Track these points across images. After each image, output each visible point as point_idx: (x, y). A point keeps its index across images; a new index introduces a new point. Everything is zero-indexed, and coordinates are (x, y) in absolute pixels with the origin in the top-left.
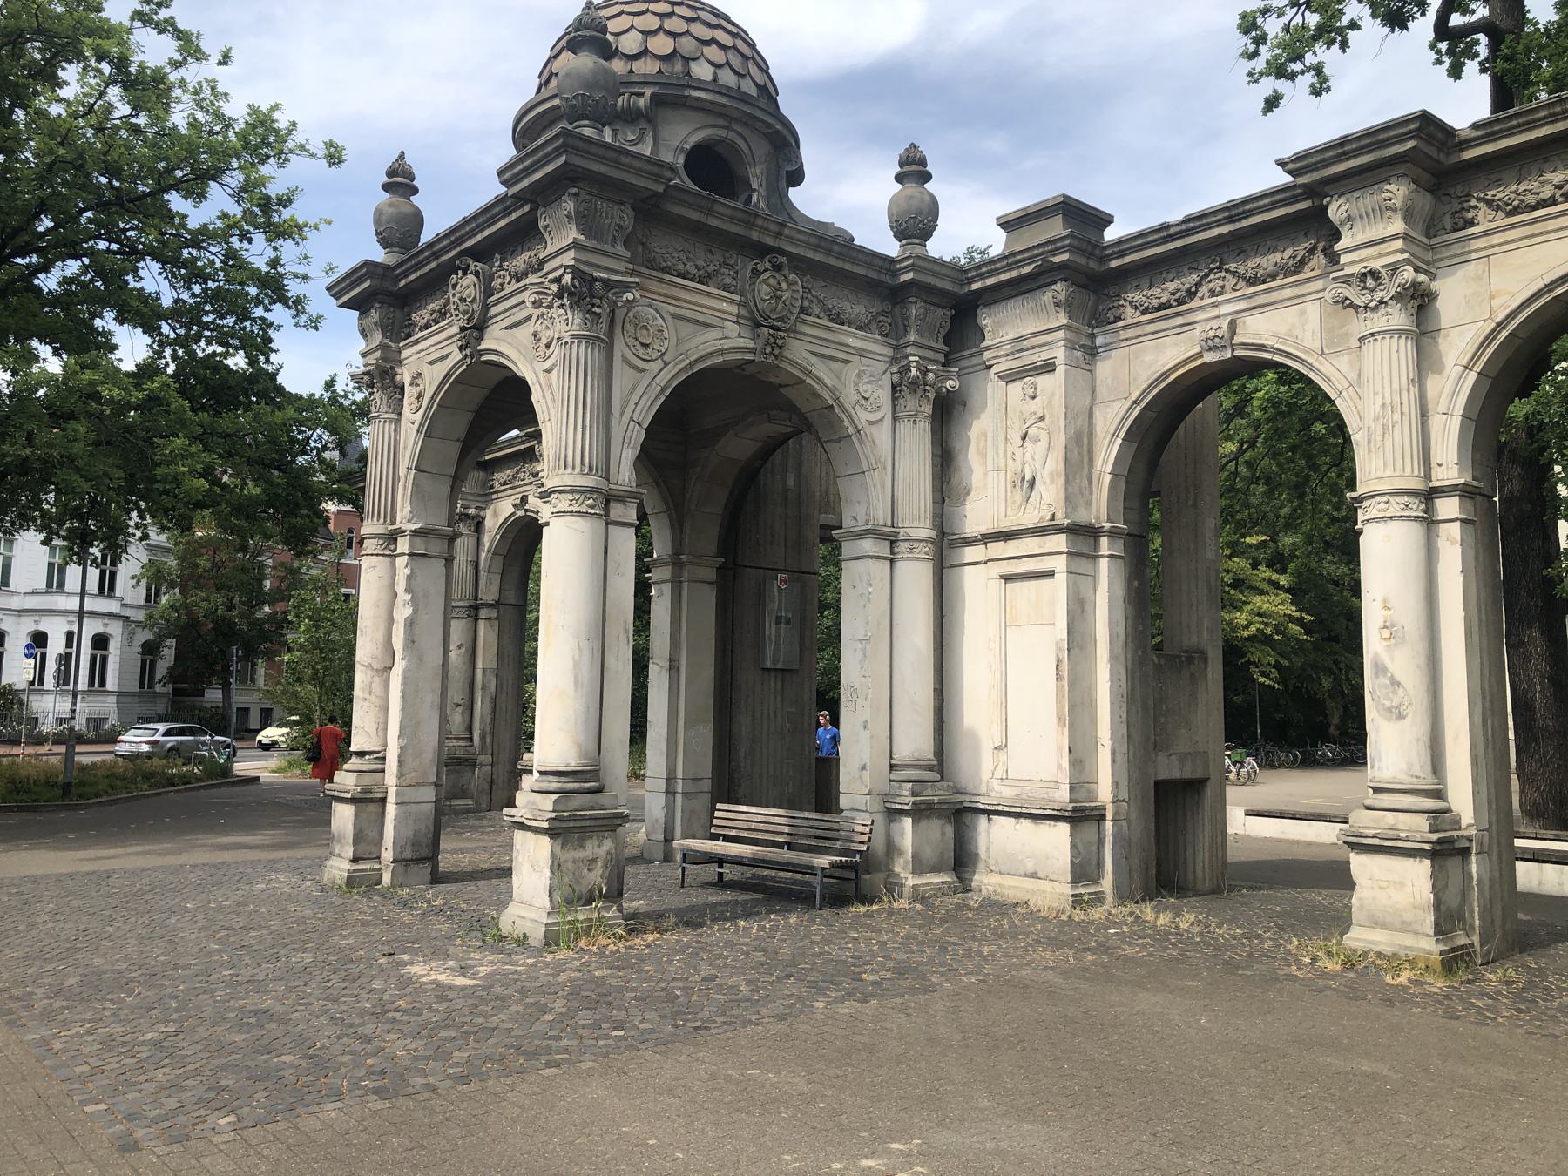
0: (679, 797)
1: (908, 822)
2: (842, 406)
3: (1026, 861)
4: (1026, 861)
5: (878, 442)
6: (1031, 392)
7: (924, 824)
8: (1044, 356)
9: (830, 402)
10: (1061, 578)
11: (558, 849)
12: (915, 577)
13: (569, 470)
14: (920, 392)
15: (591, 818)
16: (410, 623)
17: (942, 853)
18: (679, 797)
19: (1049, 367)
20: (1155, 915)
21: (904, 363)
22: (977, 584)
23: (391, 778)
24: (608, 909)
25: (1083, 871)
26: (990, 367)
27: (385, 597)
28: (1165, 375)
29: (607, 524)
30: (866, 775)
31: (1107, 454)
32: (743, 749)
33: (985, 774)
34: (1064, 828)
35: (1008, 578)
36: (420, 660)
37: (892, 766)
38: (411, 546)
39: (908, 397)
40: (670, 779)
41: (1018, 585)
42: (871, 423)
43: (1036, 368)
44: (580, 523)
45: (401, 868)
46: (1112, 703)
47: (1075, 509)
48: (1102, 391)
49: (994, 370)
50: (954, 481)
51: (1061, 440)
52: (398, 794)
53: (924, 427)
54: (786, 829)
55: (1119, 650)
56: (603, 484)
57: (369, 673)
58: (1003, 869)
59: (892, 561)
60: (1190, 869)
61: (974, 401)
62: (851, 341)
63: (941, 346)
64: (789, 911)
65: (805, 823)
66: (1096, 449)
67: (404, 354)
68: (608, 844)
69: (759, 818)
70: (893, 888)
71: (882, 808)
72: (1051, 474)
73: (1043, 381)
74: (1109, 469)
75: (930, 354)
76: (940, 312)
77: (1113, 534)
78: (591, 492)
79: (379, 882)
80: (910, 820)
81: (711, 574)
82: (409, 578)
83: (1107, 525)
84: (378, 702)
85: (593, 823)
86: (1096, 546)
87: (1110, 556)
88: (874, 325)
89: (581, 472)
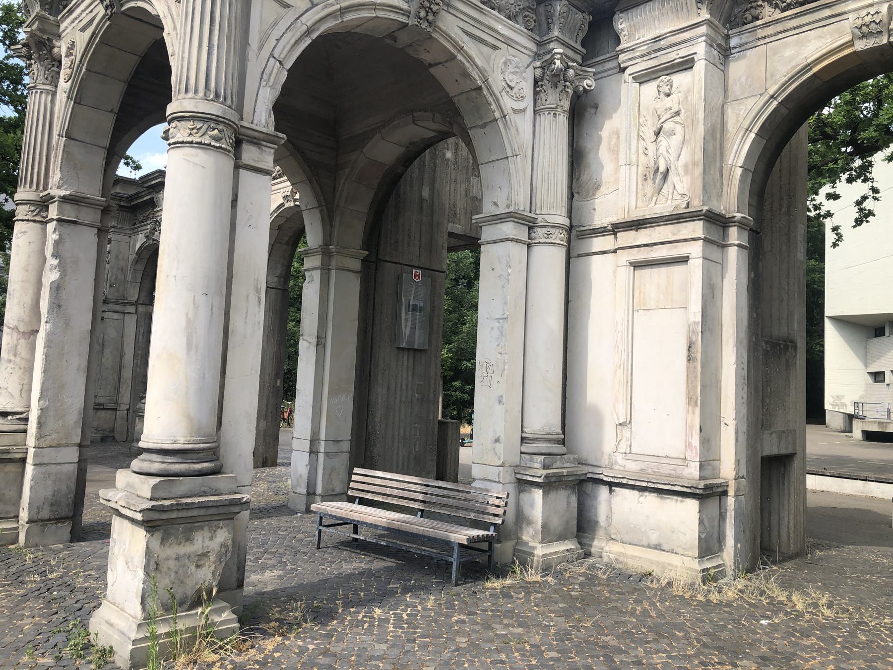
0: (321, 457)
1: (538, 495)
2: (490, 89)
3: (655, 535)
4: (655, 535)
5: (520, 130)
6: (666, 89)
7: (552, 495)
8: (683, 53)
9: (479, 83)
10: (696, 265)
11: (156, 544)
12: (550, 259)
13: (191, 94)
14: (560, 87)
15: (201, 506)
16: (57, 288)
17: (567, 522)
18: (321, 457)
19: (687, 64)
20: (769, 584)
21: (548, 57)
22: (606, 272)
23: (31, 440)
24: (219, 611)
25: (709, 546)
26: (623, 70)
27: (34, 261)
28: (808, 67)
29: (237, 167)
30: (500, 447)
31: (739, 149)
32: (379, 414)
33: (608, 445)
34: (692, 505)
35: (637, 265)
36: (67, 324)
37: (522, 439)
38: (60, 211)
39: (550, 91)
40: (314, 441)
41: (647, 272)
42: (516, 111)
43: (673, 66)
44: (201, 156)
45: (36, 528)
46: (737, 385)
47: (709, 198)
48: (735, 89)
49: (628, 71)
50: (584, 177)
51: (701, 130)
52: (36, 455)
53: (563, 121)
54: (420, 497)
55: (744, 336)
56: (232, 115)
57: (15, 335)
58: (625, 538)
59: (529, 246)
60: (774, 533)
61: (606, 102)
62: (499, 27)
63: (578, 46)
64: (427, 589)
65: (439, 492)
66: (727, 145)
67: (63, 26)
68: (223, 536)
69: (394, 484)
70: (523, 558)
71: (513, 479)
72: (686, 167)
73: (680, 80)
74: (741, 162)
75: (570, 53)
76: (580, 16)
77: (742, 225)
78: (217, 122)
79: (16, 541)
80: (540, 492)
81: (356, 265)
82: (57, 243)
83: (739, 215)
84: (23, 364)
85: (202, 512)
86: (725, 235)
87: (739, 246)
88: (520, 19)
89: (206, 98)
